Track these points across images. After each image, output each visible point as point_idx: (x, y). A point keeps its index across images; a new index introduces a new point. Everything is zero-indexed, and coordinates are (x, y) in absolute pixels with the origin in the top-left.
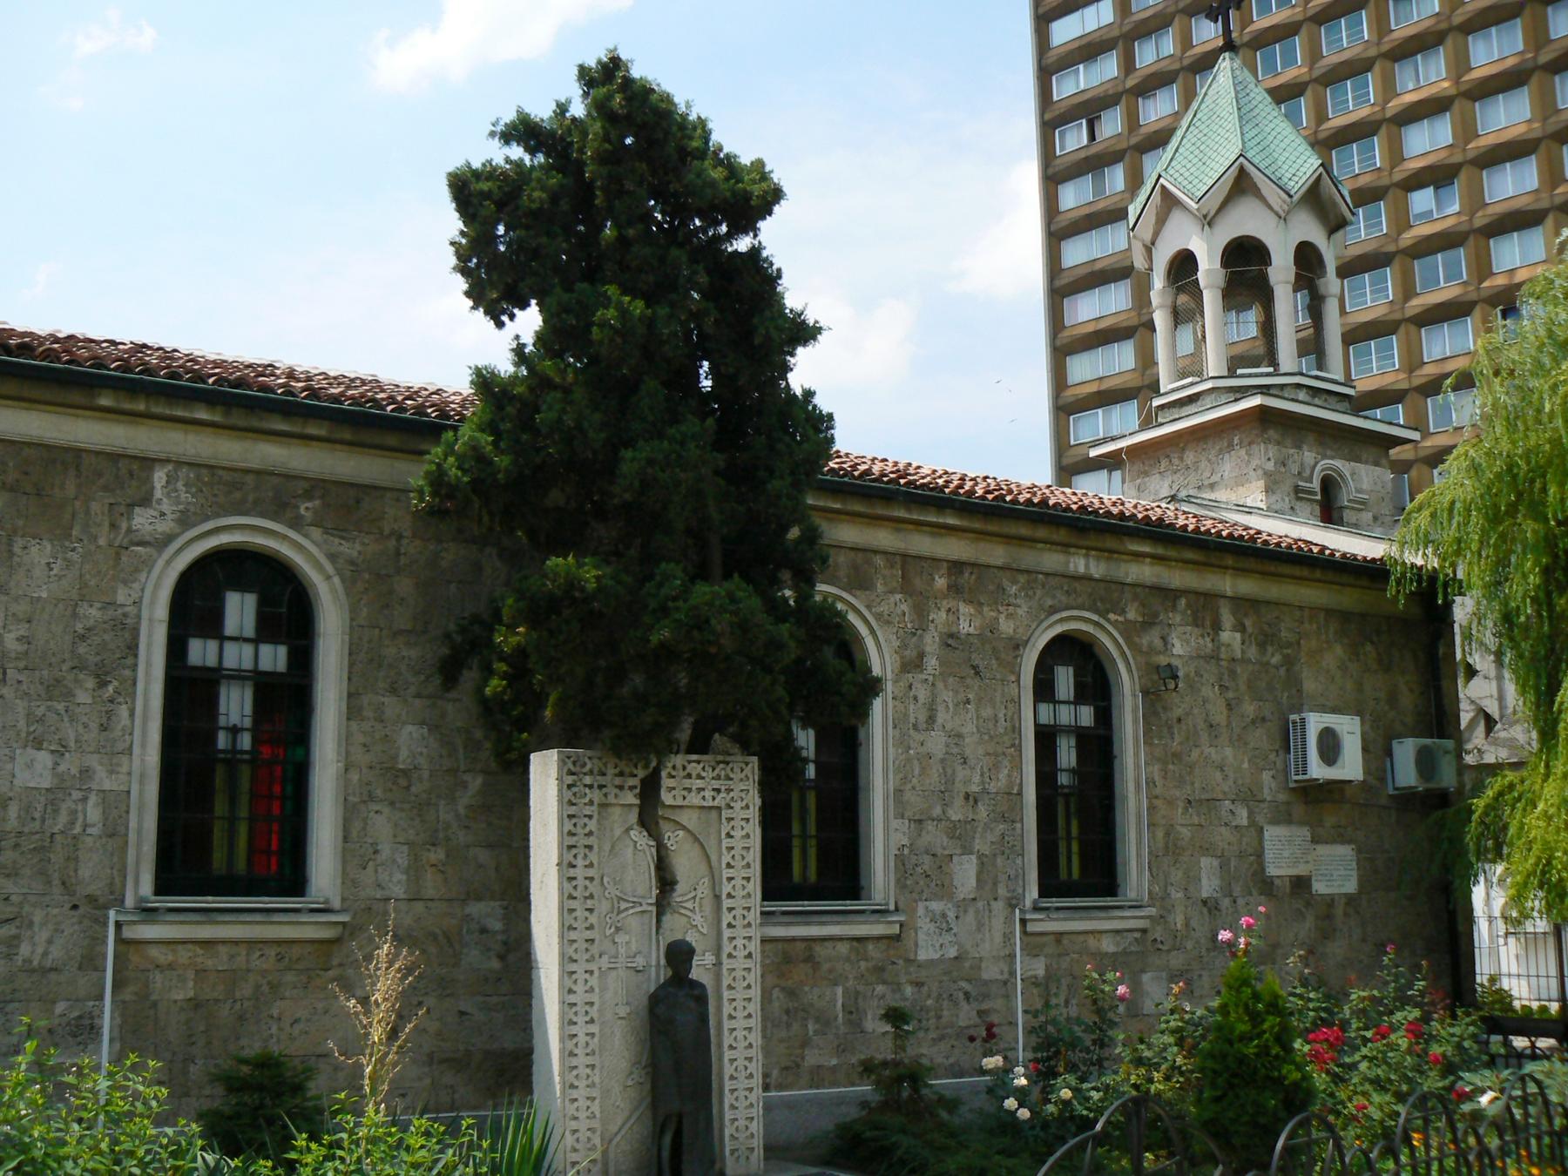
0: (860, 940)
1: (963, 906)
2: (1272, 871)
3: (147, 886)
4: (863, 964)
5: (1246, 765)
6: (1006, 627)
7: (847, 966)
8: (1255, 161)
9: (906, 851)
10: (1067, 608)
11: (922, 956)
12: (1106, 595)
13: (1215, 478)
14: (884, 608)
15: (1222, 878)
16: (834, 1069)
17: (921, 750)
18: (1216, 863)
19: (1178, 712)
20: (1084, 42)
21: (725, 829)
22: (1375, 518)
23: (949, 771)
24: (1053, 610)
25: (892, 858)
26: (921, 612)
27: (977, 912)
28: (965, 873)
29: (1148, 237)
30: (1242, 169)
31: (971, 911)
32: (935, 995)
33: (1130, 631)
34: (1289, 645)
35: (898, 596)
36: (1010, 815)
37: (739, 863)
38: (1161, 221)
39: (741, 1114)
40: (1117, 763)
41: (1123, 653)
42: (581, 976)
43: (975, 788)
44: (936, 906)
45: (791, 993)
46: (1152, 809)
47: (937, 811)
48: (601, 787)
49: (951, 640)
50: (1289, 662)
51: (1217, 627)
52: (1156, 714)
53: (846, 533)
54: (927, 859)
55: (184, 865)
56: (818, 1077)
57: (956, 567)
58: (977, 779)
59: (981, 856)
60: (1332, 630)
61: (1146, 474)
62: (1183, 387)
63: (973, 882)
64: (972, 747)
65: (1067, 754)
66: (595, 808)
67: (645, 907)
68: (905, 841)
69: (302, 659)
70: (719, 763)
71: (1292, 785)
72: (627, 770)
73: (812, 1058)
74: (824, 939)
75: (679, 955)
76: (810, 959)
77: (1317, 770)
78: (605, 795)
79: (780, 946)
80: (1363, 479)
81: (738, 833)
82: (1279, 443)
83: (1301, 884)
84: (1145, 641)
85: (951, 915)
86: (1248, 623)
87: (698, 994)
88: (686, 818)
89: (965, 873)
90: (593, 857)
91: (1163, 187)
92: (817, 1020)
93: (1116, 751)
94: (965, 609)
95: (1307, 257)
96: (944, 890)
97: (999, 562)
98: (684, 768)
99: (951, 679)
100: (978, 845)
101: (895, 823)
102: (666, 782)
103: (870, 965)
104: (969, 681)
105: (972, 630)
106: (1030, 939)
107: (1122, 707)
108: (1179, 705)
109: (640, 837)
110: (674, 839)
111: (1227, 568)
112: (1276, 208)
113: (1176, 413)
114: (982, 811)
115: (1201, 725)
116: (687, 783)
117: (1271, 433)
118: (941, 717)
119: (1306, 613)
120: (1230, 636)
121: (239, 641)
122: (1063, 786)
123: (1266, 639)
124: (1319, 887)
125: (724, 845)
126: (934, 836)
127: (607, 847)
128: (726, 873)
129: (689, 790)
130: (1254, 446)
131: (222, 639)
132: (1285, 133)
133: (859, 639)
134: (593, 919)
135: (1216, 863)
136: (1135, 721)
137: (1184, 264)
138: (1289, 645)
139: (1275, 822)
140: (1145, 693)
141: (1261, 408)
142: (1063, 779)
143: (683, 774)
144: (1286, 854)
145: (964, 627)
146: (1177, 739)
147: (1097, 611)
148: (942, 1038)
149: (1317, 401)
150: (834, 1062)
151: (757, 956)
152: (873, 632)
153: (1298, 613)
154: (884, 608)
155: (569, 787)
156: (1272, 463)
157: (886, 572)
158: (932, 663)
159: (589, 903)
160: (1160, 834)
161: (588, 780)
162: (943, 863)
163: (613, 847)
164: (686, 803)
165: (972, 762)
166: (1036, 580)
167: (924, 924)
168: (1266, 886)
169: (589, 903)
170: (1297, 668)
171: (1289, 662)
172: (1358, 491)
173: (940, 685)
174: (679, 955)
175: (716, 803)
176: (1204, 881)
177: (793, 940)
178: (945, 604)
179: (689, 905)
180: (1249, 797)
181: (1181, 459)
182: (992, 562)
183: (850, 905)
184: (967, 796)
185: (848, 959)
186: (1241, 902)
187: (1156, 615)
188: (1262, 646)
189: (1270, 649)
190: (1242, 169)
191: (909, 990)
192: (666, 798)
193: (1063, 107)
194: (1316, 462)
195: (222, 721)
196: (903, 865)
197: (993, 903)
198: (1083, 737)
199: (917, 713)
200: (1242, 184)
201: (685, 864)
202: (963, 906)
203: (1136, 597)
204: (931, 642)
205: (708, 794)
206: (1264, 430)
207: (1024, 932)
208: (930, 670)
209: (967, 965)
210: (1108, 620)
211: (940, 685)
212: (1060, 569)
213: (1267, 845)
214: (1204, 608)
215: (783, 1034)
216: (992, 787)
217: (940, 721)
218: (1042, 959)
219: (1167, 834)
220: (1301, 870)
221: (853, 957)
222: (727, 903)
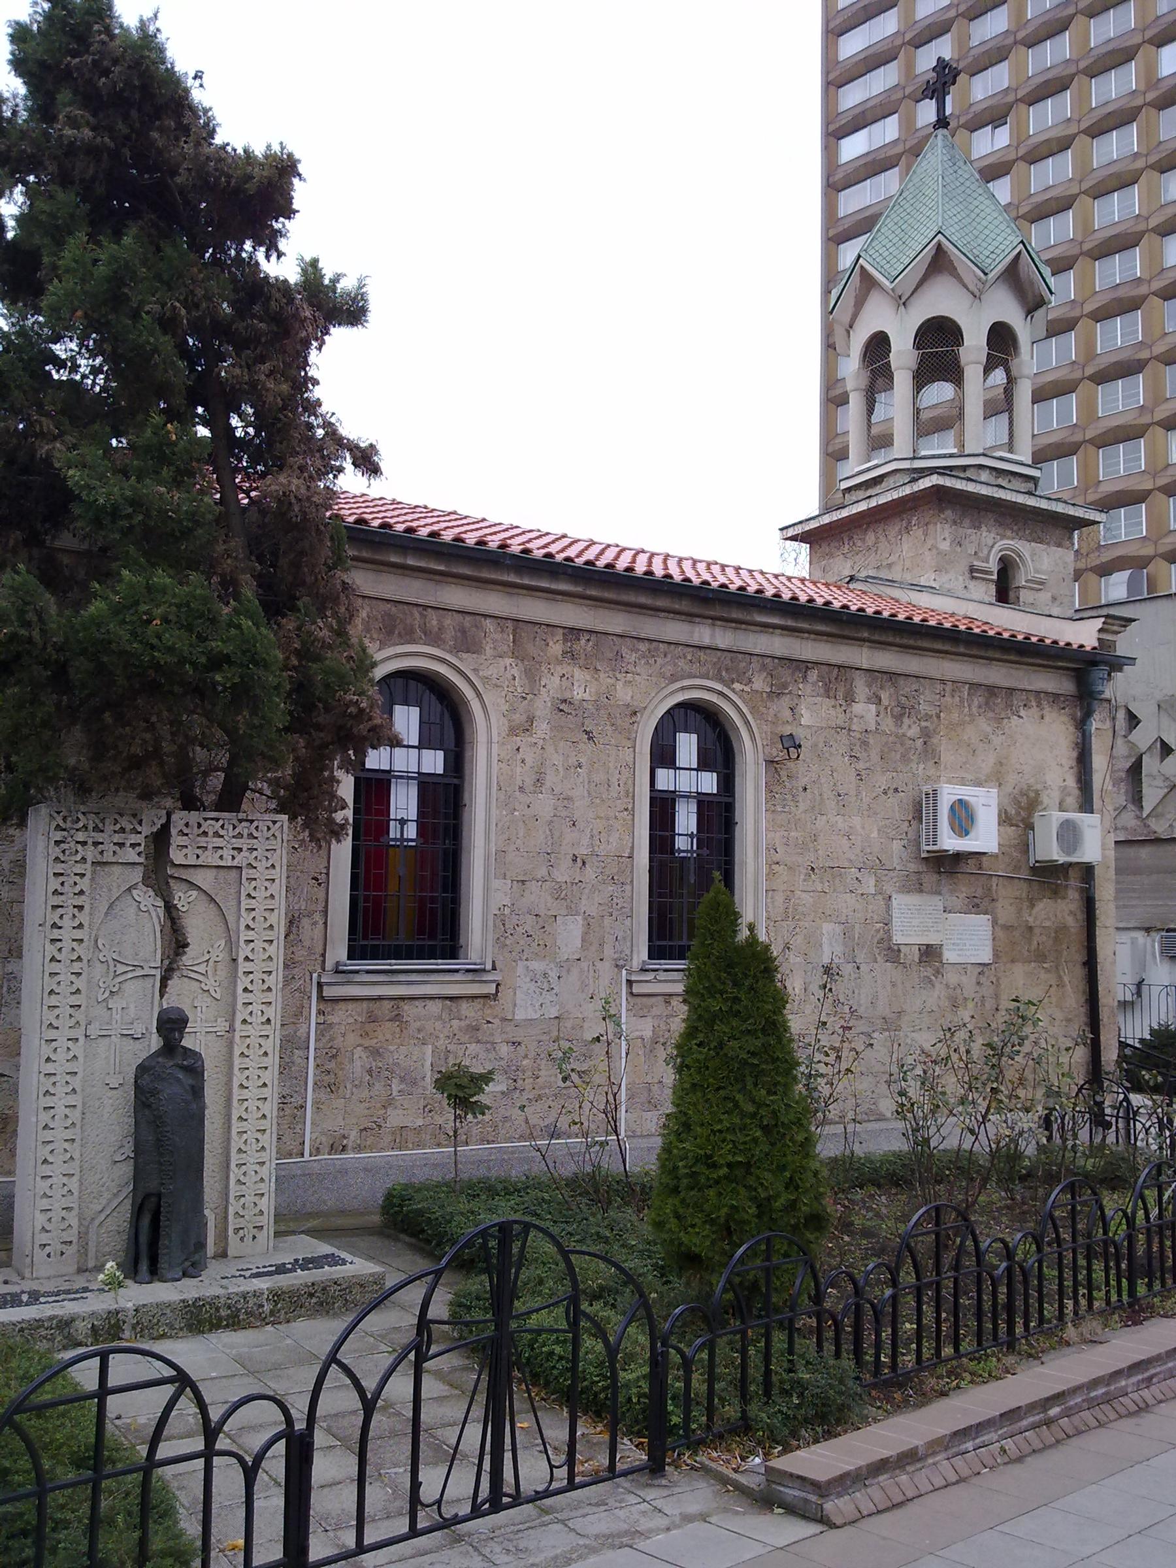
0: (451, 998)
1: (565, 966)
2: (898, 938)
3: (644, 955)
4: (455, 1023)
5: (875, 834)
6: (624, 694)
7: (438, 1025)
8: (954, 238)
9: (507, 911)
10: (691, 676)
11: (520, 1015)
12: (731, 666)
13: (893, 559)
14: (492, 672)
15: (845, 945)
16: (418, 1130)
17: (527, 812)
18: (839, 929)
19: (803, 781)
20: (869, 159)
21: (247, 888)
22: (1054, 599)
23: (557, 834)
24: (674, 678)
25: (491, 917)
26: (531, 676)
27: (582, 971)
28: (569, 935)
29: (847, 319)
30: (939, 246)
31: (575, 972)
32: (532, 1055)
33: (753, 699)
34: (928, 717)
35: (508, 661)
36: (620, 879)
37: (259, 925)
38: (859, 304)
39: (249, 1191)
40: (737, 828)
41: (747, 723)
42: (62, 1043)
43: (583, 851)
44: (537, 966)
45: (375, 1053)
46: (771, 874)
47: (542, 872)
48: (96, 844)
49: (563, 705)
50: (926, 734)
51: (850, 698)
52: (780, 782)
53: (363, 581)
54: (530, 919)
55: (371, 935)
56: (401, 1138)
57: (573, 633)
58: (585, 841)
59: (587, 918)
60: (976, 703)
61: (831, 555)
62: (869, 469)
63: (578, 943)
64: (581, 810)
65: (686, 820)
66: (88, 865)
67: (147, 971)
68: (507, 901)
69: (727, 783)
70: (240, 821)
71: (924, 855)
72: (129, 827)
73: (395, 1118)
74: (413, 998)
75: (172, 1025)
76: (397, 1018)
77: (950, 842)
78: (102, 853)
79: (365, 1004)
80: (1042, 561)
81: (260, 894)
82: (955, 523)
83: (930, 953)
84: (774, 707)
85: (553, 975)
86: (884, 696)
87: (193, 1067)
88: (203, 879)
89: (569, 935)
90: (84, 917)
91: (862, 267)
92: (402, 1079)
93: (737, 819)
94: (578, 674)
95: (1001, 340)
96: (546, 949)
97: (618, 631)
98: (199, 826)
99: (562, 743)
100: (584, 905)
101: (496, 883)
102: (176, 840)
103: (463, 1024)
104: (581, 746)
105: (586, 696)
106: (639, 1000)
107: (744, 776)
108: (805, 770)
109: (147, 899)
110: (182, 898)
111: (864, 640)
112: (971, 287)
113: (861, 494)
114: (590, 873)
115: (828, 794)
116: (202, 841)
117: (949, 513)
118: (550, 779)
119: (949, 687)
120: (865, 710)
121: (691, 779)
122: (680, 851)
123: (902, 712)
124: (949, 956)
125: (243, 906)
126: (538, 897)
127: (104, 907)
128: (245, 935)
129: (240, 850)
130: (931, 527)
131: (676, 768)
132: (988, 211)
133: (465, 703)
134: (80, 983)
135: (839, 929)
136: (757, 788)
137: (878, 345)
138: (928, 717)
139: (906, 889)
140: (770, 762)
141: (937, 488)
142: (681, 843)
143: (196, 831)
144: (915, 922)
145: (578, 694)
146: (802, 806)
147: (721, 680)
148: (539, 1098)
149: (1000, 481)
150: (420, 1122)
151: (277, 1022)
152: (747, 723)
153: (939, 687)
154: (492, 672)
155: (57, 843)
156: (948, 543)
157: (498, 636)
158: (542, 728)
159: (76, 967)
160: (780, 898)
161: (81, 836)
162: (545, 921)
163: (111, 906)
164: (199, 862)
165: (581, 824)
166: (657, 649)
167: (524, 983)
168: (893, 953)
169: (76, 967)
170: (935, 741)
171: (926, 734)
172: (1037, 571)
173: (550, 749)
174: (172, 1025)
175: (235, 863)
176: (826, 947)
177: (380, 998)
178: (560, 670)
179: (201, 969)
180: (879, 867)
181: (863, 540)
182: (610, 630)
183: (442, 964)
184: (575, 860)
185: (440, 1018)
186: (863, 967)
187: (785, 686)
188: (898, 718)
189: (906, 720)
190: (939, 246)
191: (504, 1050)
192: (176, 856)
193: (846, 224)
194: (992, 544)
195: (392, 817)
196: (501, 923)
197: (599, 964)
198: (704, 803)
199: (523, 775)
200: (939, 262)
201: (199, 925)
202: (565, 966)
203: (764, 667)
204: (542, 706)
205: (227, 853)
206: (941, 510)
207: (321, 998)
208: (540, 734)
209: (569, 1024)
210: (733, 690)
211: (550, 749)
212: (683, 639)
213: (895, 913)
214: (837, 677)
215: (365, 1094)
216: (602, 850)
217: (548, 784)
218: (649, 1019)
219: (788, 899)
220: (932, 939)
221: (445, 1016)
222: (243, 967)
